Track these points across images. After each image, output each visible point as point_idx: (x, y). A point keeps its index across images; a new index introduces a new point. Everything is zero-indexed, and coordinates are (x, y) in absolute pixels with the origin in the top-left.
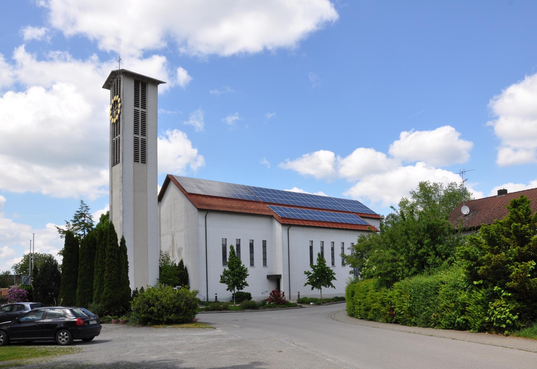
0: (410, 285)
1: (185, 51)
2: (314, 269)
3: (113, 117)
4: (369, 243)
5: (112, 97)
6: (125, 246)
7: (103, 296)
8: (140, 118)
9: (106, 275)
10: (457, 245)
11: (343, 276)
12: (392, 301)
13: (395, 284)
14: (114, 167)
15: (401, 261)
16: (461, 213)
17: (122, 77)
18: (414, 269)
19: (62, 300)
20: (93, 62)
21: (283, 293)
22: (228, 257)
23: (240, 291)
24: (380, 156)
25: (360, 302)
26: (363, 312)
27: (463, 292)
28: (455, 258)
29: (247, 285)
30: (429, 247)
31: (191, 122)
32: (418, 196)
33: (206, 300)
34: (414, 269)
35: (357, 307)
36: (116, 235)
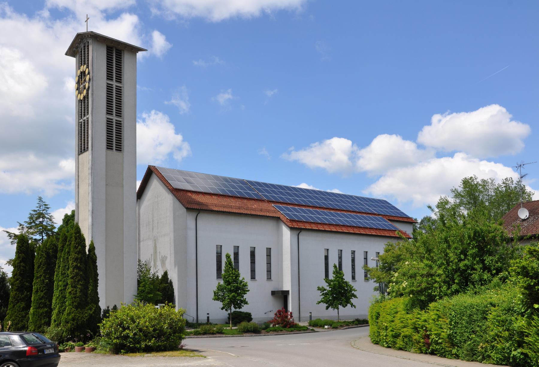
0: (450, 306)
2: (330, 284)
4: (399, 253)
7: (64, 317)
8: (114, 94)
9: (70, 290)
10: (511, 258)
11: (365, 294)
12: (428, 326)
13: (430, 305)
14: (81, 156)
15: (438, 275)
16: (518, 218)
18: (454, 287)
19: (10, 323)
20: (42, 19)
21: (291, 313)
23: (238, 310)
24: (408, 146)
25: (387, 327)
26: (390, 339)
27: (519, 317)
28: (509, 273)
29: (246, 303)
30: (474, 258)
32: (461, 195)
33: (195, 322)
34: (454, 287)
35: (383, 333)
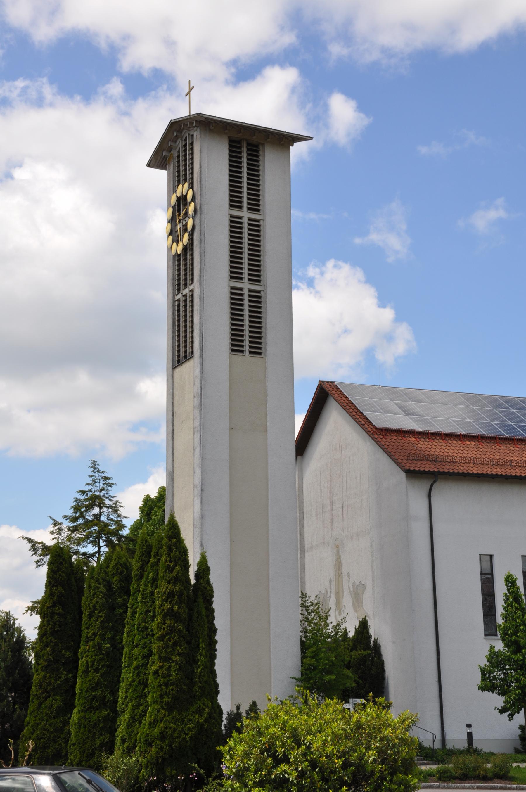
1: (345, 52)
3: (177, 241)
5: (173, 189)
6: (208, 582)
7: (143, 730)
9: (155, 667)
14: (178, 370)
17: (196, 134)
19: (31, 744)
22: (500, 610)
31: (374, 237)
33: (438, 745)
36: (185, 552)
